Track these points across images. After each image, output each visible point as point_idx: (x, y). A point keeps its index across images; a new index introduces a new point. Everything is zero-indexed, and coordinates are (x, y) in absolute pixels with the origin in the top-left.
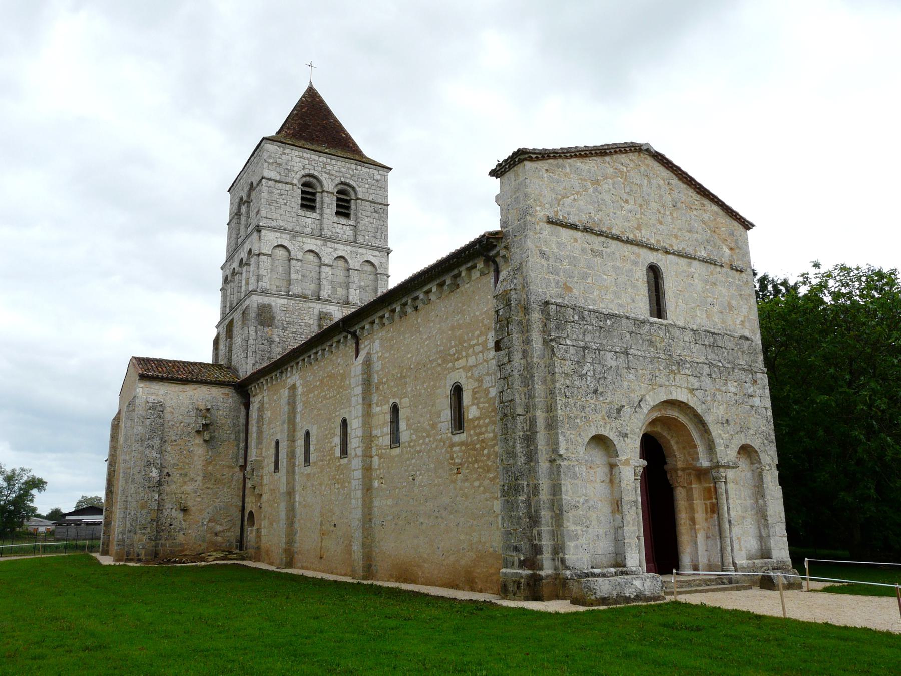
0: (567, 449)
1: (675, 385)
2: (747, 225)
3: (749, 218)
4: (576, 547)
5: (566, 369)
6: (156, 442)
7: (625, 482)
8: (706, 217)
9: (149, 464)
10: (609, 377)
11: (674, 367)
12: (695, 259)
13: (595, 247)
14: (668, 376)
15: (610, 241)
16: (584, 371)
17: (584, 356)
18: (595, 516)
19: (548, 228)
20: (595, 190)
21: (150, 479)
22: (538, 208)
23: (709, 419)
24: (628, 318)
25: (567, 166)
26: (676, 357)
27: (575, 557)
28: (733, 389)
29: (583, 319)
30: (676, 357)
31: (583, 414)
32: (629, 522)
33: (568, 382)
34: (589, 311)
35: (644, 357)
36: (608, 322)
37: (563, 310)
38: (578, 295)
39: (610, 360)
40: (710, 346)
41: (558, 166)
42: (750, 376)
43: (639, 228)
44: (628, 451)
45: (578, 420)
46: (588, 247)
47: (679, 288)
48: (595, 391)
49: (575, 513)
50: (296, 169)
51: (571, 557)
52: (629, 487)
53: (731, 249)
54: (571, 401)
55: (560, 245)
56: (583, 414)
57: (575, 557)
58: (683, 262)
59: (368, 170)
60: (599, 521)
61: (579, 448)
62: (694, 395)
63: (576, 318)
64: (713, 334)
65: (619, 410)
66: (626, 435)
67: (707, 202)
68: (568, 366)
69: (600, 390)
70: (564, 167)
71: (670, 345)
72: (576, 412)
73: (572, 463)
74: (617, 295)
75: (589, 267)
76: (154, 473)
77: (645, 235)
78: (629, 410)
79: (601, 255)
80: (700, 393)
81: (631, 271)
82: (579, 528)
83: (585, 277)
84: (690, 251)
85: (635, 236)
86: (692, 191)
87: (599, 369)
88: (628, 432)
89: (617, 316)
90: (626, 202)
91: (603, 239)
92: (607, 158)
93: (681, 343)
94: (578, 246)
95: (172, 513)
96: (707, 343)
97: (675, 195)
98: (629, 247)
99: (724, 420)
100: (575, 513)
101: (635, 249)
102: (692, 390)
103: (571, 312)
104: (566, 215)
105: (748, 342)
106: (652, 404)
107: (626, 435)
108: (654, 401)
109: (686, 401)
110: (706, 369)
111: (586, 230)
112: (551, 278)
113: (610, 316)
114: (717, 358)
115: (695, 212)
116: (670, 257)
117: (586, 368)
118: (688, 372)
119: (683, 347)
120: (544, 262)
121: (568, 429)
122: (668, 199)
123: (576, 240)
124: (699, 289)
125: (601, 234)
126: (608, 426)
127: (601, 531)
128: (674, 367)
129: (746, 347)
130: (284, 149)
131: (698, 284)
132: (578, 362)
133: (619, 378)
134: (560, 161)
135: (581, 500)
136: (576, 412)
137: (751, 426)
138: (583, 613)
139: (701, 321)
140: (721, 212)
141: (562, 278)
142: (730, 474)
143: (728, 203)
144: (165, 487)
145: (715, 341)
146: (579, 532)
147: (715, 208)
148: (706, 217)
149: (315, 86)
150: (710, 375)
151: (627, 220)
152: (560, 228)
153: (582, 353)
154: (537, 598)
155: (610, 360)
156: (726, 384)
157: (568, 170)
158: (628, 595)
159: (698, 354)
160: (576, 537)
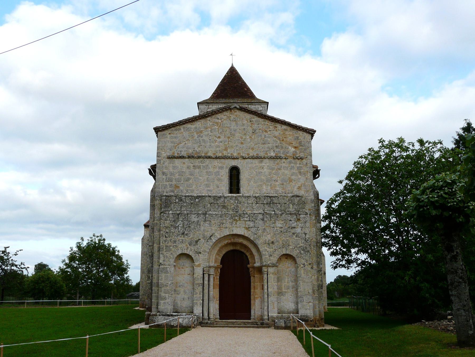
0: (164, 261)
1: (236, 227)
2: (311, 133)
3: (309, 127)
4: (165, 303)
5: (166, 225)
7: (197, 275)
8: (277, 133)
10: (192, 227)
11: (236, 218)
12: (264, 158)
13: (197, 164)
14: (232, 223)
15: (206, 159)
16: (178, 225)
17: (178, 218)
18: (183, 290)
19: (168, 161)
20: (199, 136)
22: (163, 153)
23: (259, 242)
24: (210, 196)
25: (182, 128)
26: (240, 212)
27: (163, 307)
28: (280, 225)
29: (181, 200)
30: (240, 212)
31: (175, 244)
32: (197, 293)
33: (167, 231)
34: (185, 196)
35: (216, 215)
36: (197, 200)
37: (170, 198)
38: (184, 190)
39: (194, 218)
40: (267, 204)
41: (176, 130)
42: (295, 217)
43: (226, 149)
44: (201, 260)
45: (172, 247)
46: (191, 165)
47: (252, 176)
48: (183, 234)
49: (166, 288)
51: (161, 307)
52: (199, 277)
53: (295, 147)
54: (169, 239)
55: (174, 167)
56: (175, 244)
57: (163, 307)
58: (256, 161)
59: (255, 106)
60: (185, 292)
62: (249, 231)
63: (177, 200)
64: (270, 197)
65: (197, 242)
66: (200, 253)
67: (278, 126)
69: (186, 233)
70: (180, 129)
71: (238, 206)
73: (166, 267)
74: (207, 186)
75: (191, 175)
77: (229, 152)
78: (203, 241)
79: (199, 167)
80: (253, 230)
81: (218, 172)
82: (167, 295)
83: (188, 179)
84: (262, 154)
85: (223, 154)
86: (267, 121)
87: (186, 223)
88: (201, 251)
90: (219, 137)
91: (201, 159)
92: (208, 119)
93: (246, 205)
94: (185, 166)
96: (264, 202)
97: (255, 126)
98: (218, 160)
99: (270, 242)
100: (166, 288)
101: (223, 160)
102: (248, 229)
103: (174, 198)
104: (179, 153)
105: (298, 198)
106: (219, 237)
107: (200, 253)
108: (220, 235)
109: (243, 234)
112: (167, 183)
113: (198, 197)
114: (272, 209)
115: (269, 133)
116: (246, 160)
117: (178, 223)
118: (246, 219)
119: (245, 208)
120: (164, 177)
121: (165, 252)
122: (250, 130)
123: (184, 163)
124: (267, 173)
125: (199, 157)
126: (189, 249)
127: (186, 297)
128: (236, 218)
129: (296, 201)
130: (209, 106)
131: (266, 170)
132: (174, 221)
133: (198, 226)
134: (178, 127)
135: (169, 283)
136: (170, 244)
137: (291, 244)
138: (336, 330)
140: (289, 128)
141: (174, 183)
142: (271, 270)
143: (293, 122)
145: (272, 200)
146: (167, 297)
147: (284, 127)
148: (277, 133)
149: (234, 66)
150: (263, 220)
151: (218, 146)
152: (176, 159)
153: (177, 217)
155: (194, 218)
156: (275, 223)
157: (182, 130)
158: (172, 324)
160: (165, 298)
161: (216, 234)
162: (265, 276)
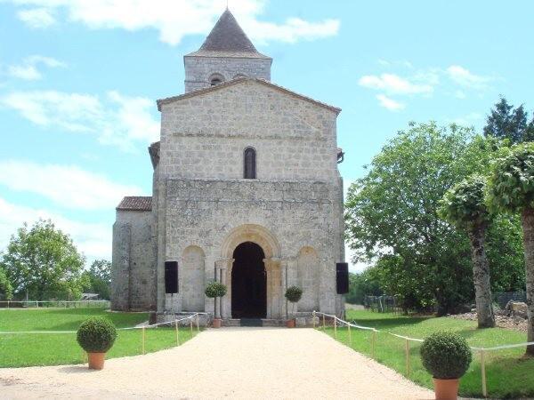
6: (126, 247)
9: (123, 258)
21: (124, 267)
36: (208, 185)
39: (204, 206)
50: (206, 72)
61: (179, 253)
65: (208, 233)
66: (212, 245)
68: (174, 211)
69: (196, 222)
72: (177, 235)
76: (126, 263)
79: (210, 148)
89: (214, 181)
95: (137, 285)
105: (321, 186)
110: (279, 205)
111: (200, 135)
112: (173, 165)
113: (209, 182)
136: (177, 235)
139: (286, 174)
144: (132, 271)
149: (230, 10)
154: (486, 377)
155: (204, 206)
159: (276, 196)
161: (229, 224)
162: (284, 271)
